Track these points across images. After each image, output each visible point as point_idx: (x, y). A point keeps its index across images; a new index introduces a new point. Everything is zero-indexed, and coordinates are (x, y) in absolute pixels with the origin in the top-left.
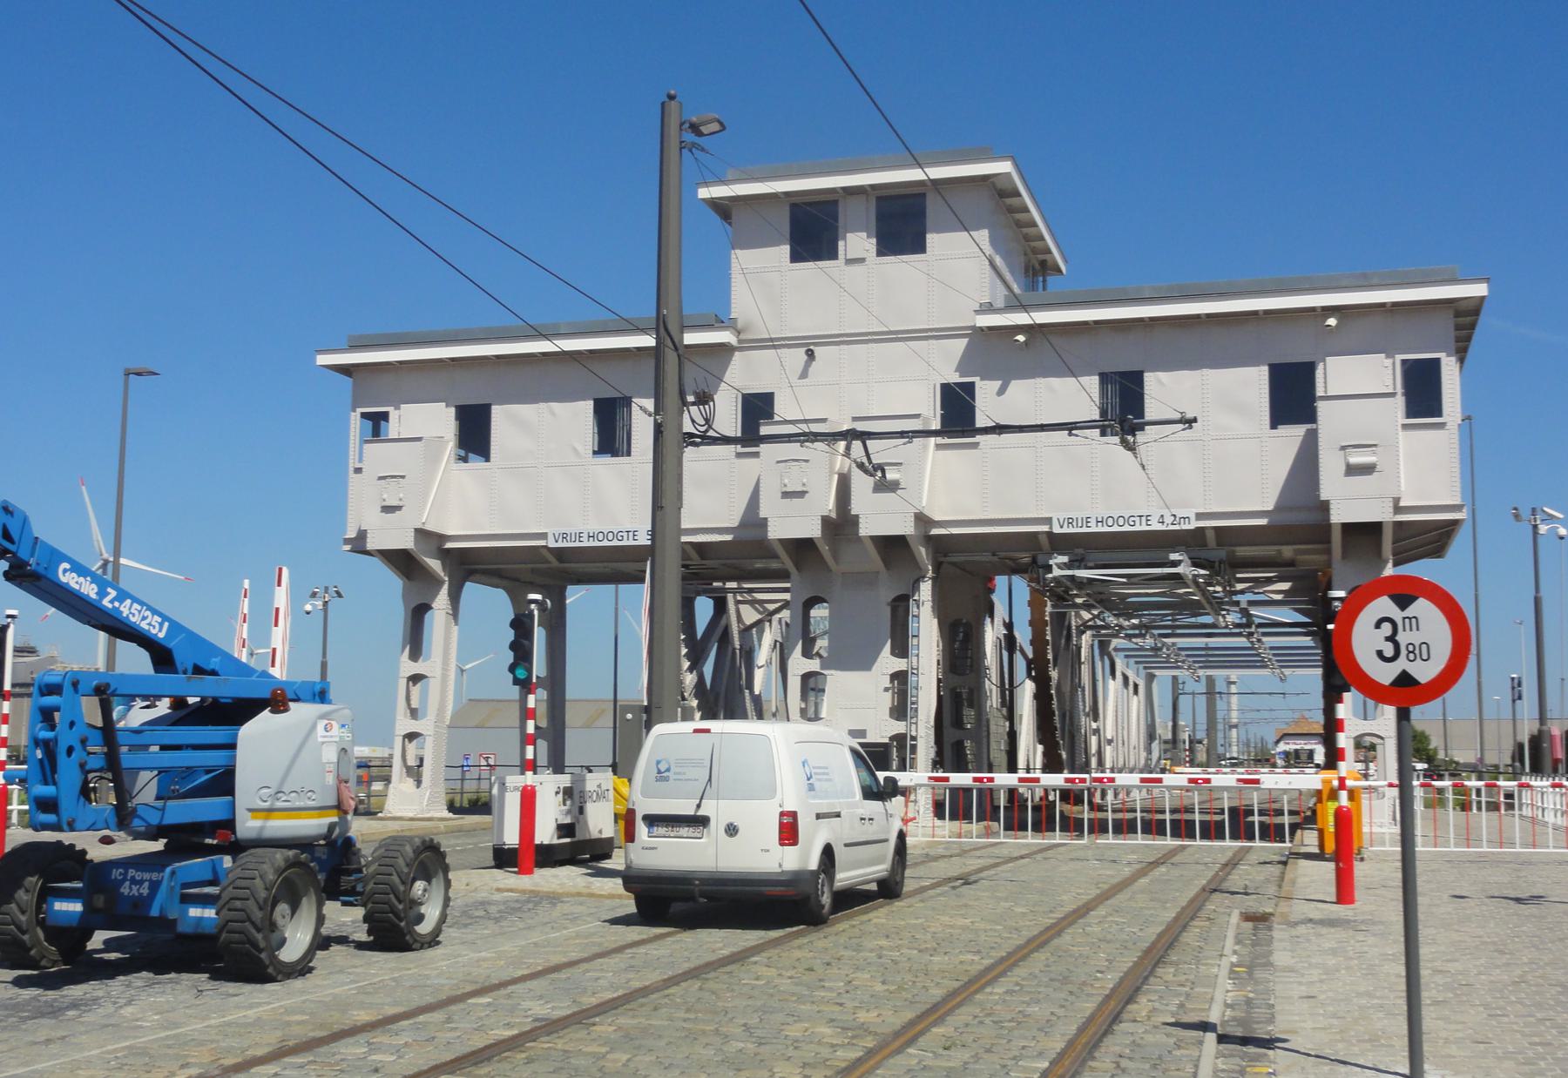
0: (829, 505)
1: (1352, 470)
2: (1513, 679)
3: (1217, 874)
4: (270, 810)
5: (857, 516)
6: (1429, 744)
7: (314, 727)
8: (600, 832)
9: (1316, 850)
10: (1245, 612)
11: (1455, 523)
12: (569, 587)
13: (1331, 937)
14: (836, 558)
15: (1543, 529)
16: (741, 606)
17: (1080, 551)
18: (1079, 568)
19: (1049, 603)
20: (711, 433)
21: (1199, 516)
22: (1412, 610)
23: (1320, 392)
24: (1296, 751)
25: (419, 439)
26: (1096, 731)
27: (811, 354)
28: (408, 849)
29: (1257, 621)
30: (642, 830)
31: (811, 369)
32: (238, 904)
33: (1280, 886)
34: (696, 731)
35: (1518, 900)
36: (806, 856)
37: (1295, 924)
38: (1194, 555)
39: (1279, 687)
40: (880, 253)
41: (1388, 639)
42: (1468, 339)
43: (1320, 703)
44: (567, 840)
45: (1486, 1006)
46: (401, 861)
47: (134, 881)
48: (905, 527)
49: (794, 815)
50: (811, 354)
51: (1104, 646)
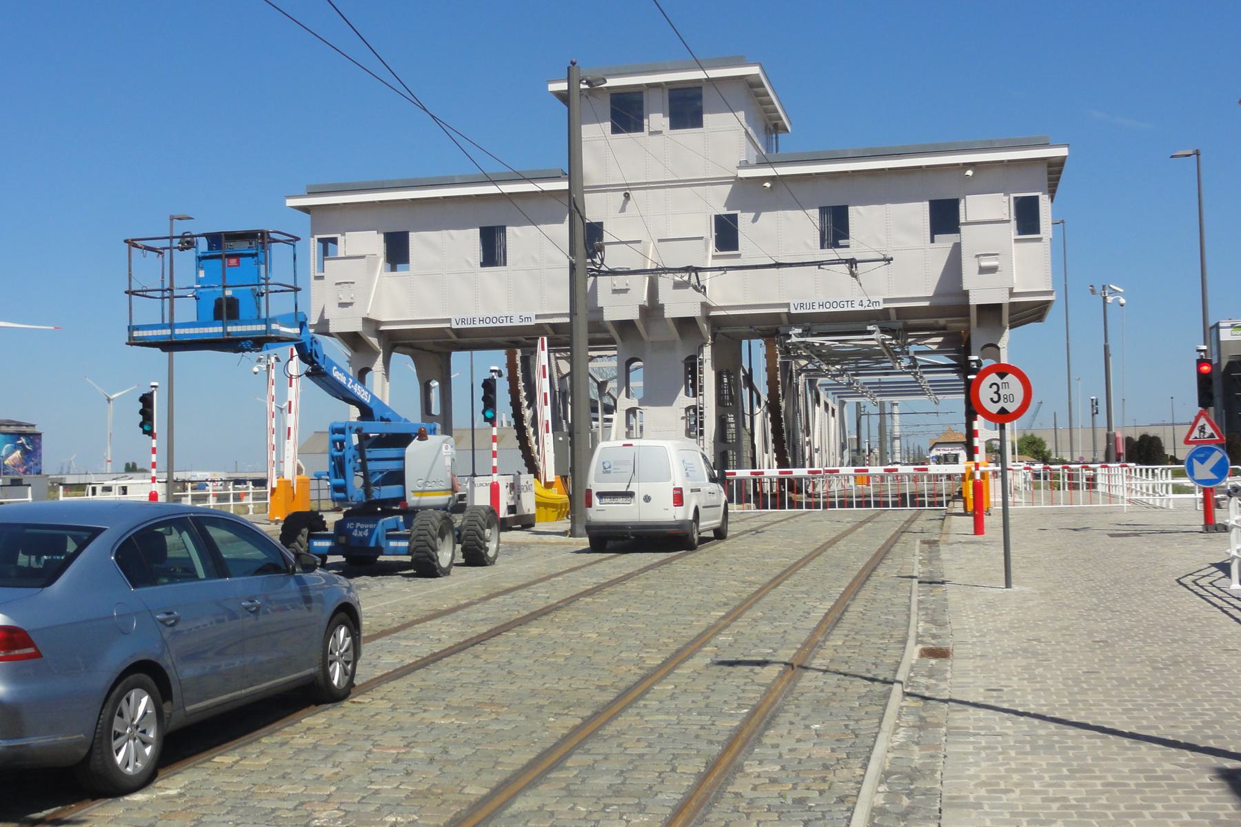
0: (644, 298)
1: (983, 270)
2: (1092, 400)
3: (903, 526)
4: (422, 491)
5: (663, 305)
6: (1044, 448)
7: (440, 449)
8: (529, 510)
9: (963, 511)
10: (913, 360)
11: (1049, 302)
12: (453, 353)
13: (971, 548)
14: (648, 332)
15: (1110, 299)
16: (559, 361)
17: (809, 324)
18: (807, 336)
19: (779, 356)
20: (603, 268)
21: (885, 301)
22: (1005, 380)
23: (962, 220)
24: (945, 455)
25: (363, 257)
26: (809, 443)
27: (627, 196)
28: (483, 512)
29: (920, 363)
30: (596, 500)
31: (627, 206)
32: (422, 538)
33: (942, 529)
34: (624, 445)
35: (1075, 530)
36: (687, 512)
37: (951, 544)
38: (882, 325)
39: (933, 408)
40: (674, 125)
41: (995, 393)
42: (1056, 185)
43: (964, 420)
44: (513, 515)
45: (1045, 567)
46: (480, 518)
47: (359, 529)
48: (695, 312)
49: (681, 489)
50: (627, 196)
51: (812, 383)
